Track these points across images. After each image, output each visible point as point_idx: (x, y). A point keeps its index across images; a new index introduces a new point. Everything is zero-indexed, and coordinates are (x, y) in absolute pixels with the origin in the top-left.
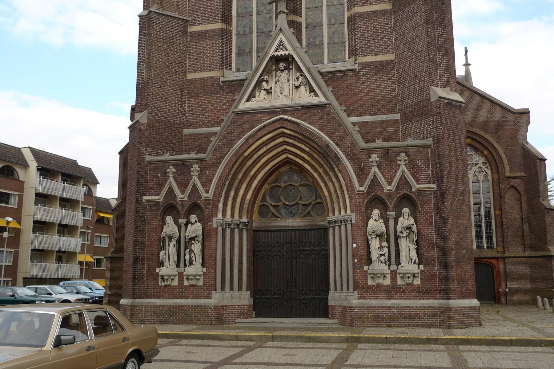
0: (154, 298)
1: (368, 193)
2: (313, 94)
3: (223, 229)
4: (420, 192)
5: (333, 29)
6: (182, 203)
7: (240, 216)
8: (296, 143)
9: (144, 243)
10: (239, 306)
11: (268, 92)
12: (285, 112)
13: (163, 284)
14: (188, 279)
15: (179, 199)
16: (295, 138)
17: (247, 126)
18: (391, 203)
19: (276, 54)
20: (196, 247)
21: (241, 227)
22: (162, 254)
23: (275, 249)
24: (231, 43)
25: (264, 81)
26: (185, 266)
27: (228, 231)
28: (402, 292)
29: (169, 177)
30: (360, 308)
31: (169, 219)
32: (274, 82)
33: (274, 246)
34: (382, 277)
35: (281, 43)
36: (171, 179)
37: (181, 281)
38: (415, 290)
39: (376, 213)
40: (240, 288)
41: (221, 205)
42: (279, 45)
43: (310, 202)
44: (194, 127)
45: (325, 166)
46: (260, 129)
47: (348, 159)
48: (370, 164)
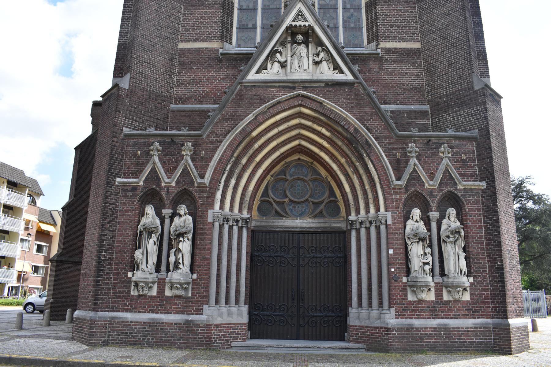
0: (123, 311)
1: (407, 188)
2: (337, 71)
3: (220, 225)
4: (466, 191)
5: (348, 13)
6: (168, 190)
7: (240, 211)
8: (316, 127)
9: (113, 238)
10: (237, 324)
11: (283, 65)
12: (305, 88)
13: (136, 293)
14: (171, 288)
15: (163, 184)
16: (314, 120)
17: (257, 101)
18: (433, 201)
19: (294, 24)
20: (185, 246)
21: (240, 225)
22: (138, 254)
23: (267, 254)
24: (232, 16)
25: (279, 52)
26: (168, 270)
27: (226, 227)
28: (449, 310)
29: (152, 156)
30: (399, 329)
31: (150, 210)
32: (289, 55)
33: (277, 251)
34: (426, 290)
35: (300, 13)
36: (156, 159)
37: (161, 290)
38: (463, 307)
39: (416, 213)
40: (237, 302)
41: (219, 195)
42: (298, 15)
43: (322, 199)
44: (184, 102)
45: (350, 155)
46: (274, 105)
47: (382, 148)
48: (408, 154)
